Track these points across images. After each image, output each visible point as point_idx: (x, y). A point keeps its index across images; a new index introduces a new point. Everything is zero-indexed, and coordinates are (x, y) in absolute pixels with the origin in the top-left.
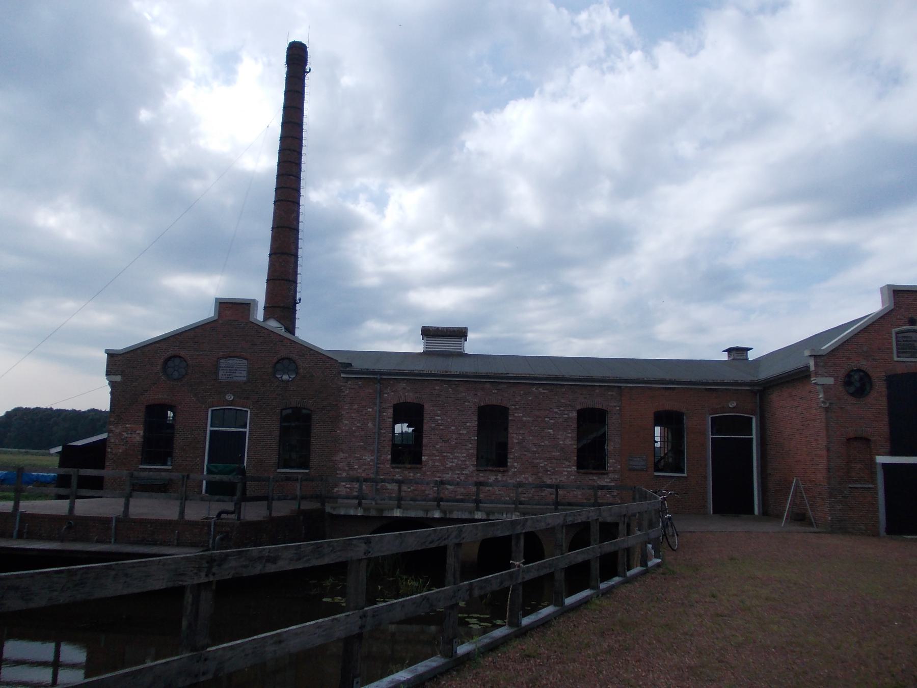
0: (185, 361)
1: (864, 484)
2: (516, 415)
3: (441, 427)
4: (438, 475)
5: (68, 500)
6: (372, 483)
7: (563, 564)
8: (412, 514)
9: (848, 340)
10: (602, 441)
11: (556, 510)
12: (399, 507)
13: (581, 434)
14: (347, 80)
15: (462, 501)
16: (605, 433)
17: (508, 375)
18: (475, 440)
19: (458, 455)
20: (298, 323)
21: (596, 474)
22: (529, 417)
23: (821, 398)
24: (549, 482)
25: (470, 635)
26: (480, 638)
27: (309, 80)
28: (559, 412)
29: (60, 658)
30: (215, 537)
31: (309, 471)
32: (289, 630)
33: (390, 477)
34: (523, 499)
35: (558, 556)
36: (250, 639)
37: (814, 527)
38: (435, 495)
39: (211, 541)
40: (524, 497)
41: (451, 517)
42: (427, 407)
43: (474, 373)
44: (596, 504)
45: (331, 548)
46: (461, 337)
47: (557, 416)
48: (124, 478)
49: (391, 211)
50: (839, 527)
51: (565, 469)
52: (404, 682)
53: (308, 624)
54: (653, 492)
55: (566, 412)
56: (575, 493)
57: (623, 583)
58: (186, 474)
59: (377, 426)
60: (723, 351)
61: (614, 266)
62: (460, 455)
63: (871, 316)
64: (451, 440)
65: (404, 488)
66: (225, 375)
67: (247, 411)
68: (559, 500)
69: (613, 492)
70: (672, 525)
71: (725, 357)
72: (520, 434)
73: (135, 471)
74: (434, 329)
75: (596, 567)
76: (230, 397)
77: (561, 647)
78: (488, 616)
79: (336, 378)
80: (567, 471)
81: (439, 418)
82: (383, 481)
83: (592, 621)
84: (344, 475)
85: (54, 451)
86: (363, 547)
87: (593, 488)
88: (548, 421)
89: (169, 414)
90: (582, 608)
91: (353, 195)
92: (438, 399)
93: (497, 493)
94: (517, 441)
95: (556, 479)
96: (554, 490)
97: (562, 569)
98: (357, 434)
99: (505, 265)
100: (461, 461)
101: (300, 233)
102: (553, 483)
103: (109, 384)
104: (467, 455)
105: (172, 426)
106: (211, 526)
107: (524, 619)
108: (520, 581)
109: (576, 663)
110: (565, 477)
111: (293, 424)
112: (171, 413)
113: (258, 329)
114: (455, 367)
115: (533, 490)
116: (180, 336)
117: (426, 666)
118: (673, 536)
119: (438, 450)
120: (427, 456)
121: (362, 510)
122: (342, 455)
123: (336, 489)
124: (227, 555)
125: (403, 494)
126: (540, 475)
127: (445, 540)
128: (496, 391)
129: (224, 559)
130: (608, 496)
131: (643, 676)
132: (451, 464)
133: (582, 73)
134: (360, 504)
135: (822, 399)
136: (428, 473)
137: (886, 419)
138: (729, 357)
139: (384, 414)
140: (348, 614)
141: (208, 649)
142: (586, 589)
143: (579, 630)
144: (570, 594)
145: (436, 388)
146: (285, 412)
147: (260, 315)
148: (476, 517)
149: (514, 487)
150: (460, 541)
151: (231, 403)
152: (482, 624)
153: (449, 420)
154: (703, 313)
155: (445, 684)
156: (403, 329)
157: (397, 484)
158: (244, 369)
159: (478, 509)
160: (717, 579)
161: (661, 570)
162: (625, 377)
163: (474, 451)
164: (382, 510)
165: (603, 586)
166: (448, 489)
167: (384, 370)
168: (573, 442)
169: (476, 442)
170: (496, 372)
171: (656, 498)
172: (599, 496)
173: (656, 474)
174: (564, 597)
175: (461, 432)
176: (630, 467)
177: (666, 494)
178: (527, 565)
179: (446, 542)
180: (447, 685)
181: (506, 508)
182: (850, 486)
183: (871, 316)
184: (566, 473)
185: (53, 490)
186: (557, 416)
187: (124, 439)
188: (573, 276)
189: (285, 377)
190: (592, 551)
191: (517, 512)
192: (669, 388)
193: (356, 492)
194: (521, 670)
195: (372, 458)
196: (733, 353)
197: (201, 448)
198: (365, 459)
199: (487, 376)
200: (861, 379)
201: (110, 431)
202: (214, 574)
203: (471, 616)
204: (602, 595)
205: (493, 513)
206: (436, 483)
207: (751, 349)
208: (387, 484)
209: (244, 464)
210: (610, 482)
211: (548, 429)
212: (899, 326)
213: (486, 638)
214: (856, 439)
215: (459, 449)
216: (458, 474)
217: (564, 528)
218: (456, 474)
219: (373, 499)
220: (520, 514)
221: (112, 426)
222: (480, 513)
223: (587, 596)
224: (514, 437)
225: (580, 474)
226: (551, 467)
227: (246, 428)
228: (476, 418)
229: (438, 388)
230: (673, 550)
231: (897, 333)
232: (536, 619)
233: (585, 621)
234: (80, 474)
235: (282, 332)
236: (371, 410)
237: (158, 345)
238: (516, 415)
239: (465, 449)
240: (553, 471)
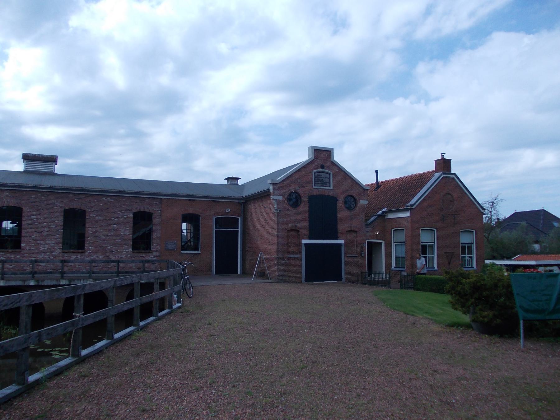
1: (295, 255)
2: (91, 215)
3: (36, 223)
4: (34, 256)
7: (114, 312)
8: (13, 284)
9: (290, 175)
11: (118, 276)
15: (51, 273)
16: (151, 228)
17: (85, 189)
18: (61, 232)
19: (48, 242)
21: (145, 253)
22: (101, 217)
23: (275, 207)
24: (113, 259)
28: (121, 214)
34: (96, 270)
37: (269, 279)
38: (31, 270)
40: (96, 269)
41: (43, 284)
43: (61, 186)
47: (120, 216)
50: (282, 279)
51: (125, 250)
54: (179, 263)
56: (131, 265)
57: (155, 321)
60: (225, 179)
61: (170, 120)
62: (50, 242)
63: (302, 163)
64: (44, 232)
65: (7, 265)
68: (119, 270)
69: (155, 264)
70: (189, 282)
71: (225, 182)
74: (32, 155)
75: (137, 312)
77: (108, 367)
78: (67, 349)
87: (142, 261)
88: (113, 219)
90: (126, 339)
92: (34, 204)
94: (91, 233)
95: (118, 257)
97: (113, 315)
100: (51, 246)
104: (56, 243)
108: (80, 326)
110: (125, 255)
114: (47, 182)
118: (190, 289)
127: (17, 303)
130: (152, 266)
131: (160, 380)
132: (43, 248)
135: (276, 208)
136: (25, 255)
137: (307, 219)
138: (228, 183)
142: (130, 327)
145: (32, 196)
148: (61, 283)
149: (89, 262)
150: (30, 303)
152: (61, 354)
153: (42, 218)
154: (222, 155)
159: (62, 278)
160: (213, 313)
161: (180, 310)
162: (165, 192)
163: (60, 240)
165: (142, 324)
168: (130, 233)
169: (62, 233)
170: (77, 187)
171: (180, 267)
173: (182, 252)
174: (113, 334)
176: (167, 248)
177: (186, 264)
179: (18, 305)
182: (288, 256)
183: (302, 163)
184: (125, 253)
186: (120, 216)
188: (144, 125)
190: (136, 302)
192: (191, 200)
196: (231, 180)
199: (71, 189)
200: (296, 197)
203: (54, 350)
204: (141, 330)
205: (74, 280)
206: (31, 262)
207: (241, 178)
210: (154, 258)
211: (114, 225)
212: (316, 169)
213: (53, 367)
214: (292, 230)
215: (50, 238)
217: (115, 289)
220: (93, 280)
223: (131, 331)
224: (90, 230)
225: (135, 253)
226: (115, 249)
228: (62, 217)
229: (34, 196)
230: (190, 297)
231: (315, 173)
232: (93, 350)
233: (127, 348)
238: (91, 215)
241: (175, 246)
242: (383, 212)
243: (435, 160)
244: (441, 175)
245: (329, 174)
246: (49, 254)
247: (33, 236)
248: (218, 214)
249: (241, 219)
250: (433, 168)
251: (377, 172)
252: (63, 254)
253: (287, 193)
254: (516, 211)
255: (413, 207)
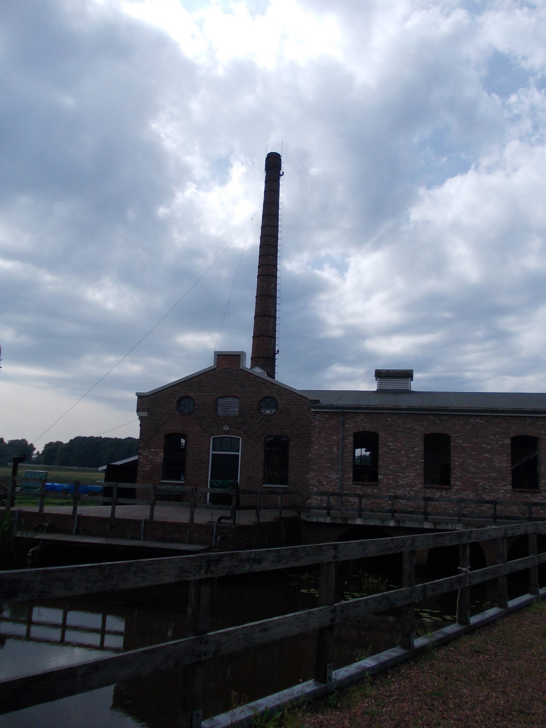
0: (193, 400)
5: (111, 506)
6: (338, 497)
8: (371, 523)
10: (534, 464)
12: (360, 516)
13: (514, 457)
14: (314, 171)
15: (412, 513)
18: (422, 462)
19: (407, 474)
20: (277, 369)
24: (487, 498)
25: (424, 629)
26: (434, 633)
27: (283, 181)
28: (495, 439)
29: (106, 627)
30: (216, 537)
31: (288, 487)
32: (272, 620)
33: (352, 492)
34: (465, 512)
35: (500, 565)
36: (241, 626)
39: (214, 540)
42: (381, 435)
44: (531, 519)
45: (305, 553)
46: (408, 377)
48: (150, 490)
49: (351, 277)
51: (502, 488)
52: (368, 669)
53: (288, 615)
55: (501, 439)
56: (511, 508)
58: (195, 487)
59: (341, 451)
62: (409, 474)
65: (364, 501)
66: (222, 411)
67: (240, 439)
72: (461, 457)
73: (158, 484)
76: (226, 428)
79: (307, 412)
80: (504, 490)
81: (392, 444)
82: (347, 495)
83: (533, 623)
84: (315, 490)
85: (101, 468)
86: (332, 552)
88: (485, 447)
89: (182, 441)
91: (319, 263)
92: (390, 428)
93: (443, 506)
95: (494, 496)
96: (492, 505)
98: (324, 457)
99: (447, 315)
100: (411, 479)
101: (278, 299)
102: (491, 499)
103: (139, 419)
105: (184, 450)
106: (213, 528)
107: (471, 618)
108: (467, 585)
109: (522, 661)
110: (502, 495)
111: (275, 449)
112: (184, 440)
113: (247, 374)
114: (404, 402)
115: (474, 504)
116: (189, 381)
117: (388, 656)
119: (391, 471)
120: (383, 475)
121: (330, 519)
122: (313, 474)
123: (309, 501)
124: (222, 556)
125: (363, 506)
126: (480, 492)
127: (400, 547)
128: (439, 422)
129: (219, 559)
133: (513, 145)
134: (328, 514)
136: (383, 489)
139: (346, 441)
140: (321, 608)
141: (209, 634)
143: (522, 630)
144: (511, 598)
146: (268, 440)
147: (248, 364)
151: (227, 432)
152: (433, 618)
153: (399, 446)
155: (404, 672)
156: (361, 371)
157: (358, 498)
158: (236, 406)
159: (426, 520)
163: (421, 472)
164: (346, 519)
166: (400, 503)
167: (345, 405)
172: (533, 512)
175: (410, 455)
178: (473, 572)
180: (406, 673)
181: (450, 519)
184: (503, 491)
185: (101, 498)
187: (150, 460)
189: (268, 412)
191: (460, 523)
193: (325, 504)
194: (472, 664)
195: (338, 476)
197: (205, 467)
198: (332, 477)
201: (139, 455)
202: (212, 572)
208: (350, 498)
209: (238, 480)
210: (543, 500)
216: (409, 490)
218: (406, 490)
219: (339, 510)
221: (141, 451)
222: (428, 523)
223: (528, 600)
224: (456, 460)
227: (239, 452)
228: (422, 444)
233: (527, 623)
234: (119, 487)
235: (265, 376)
236: (335, 437)
237: (173, 389)
238: (457, 441)
239: (414, 470)
240: (490, 489)
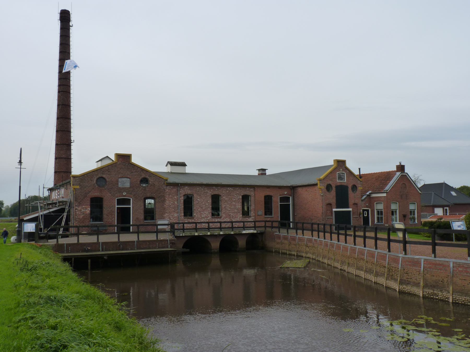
62: (206, 213)
95: (236, 219)
137: (335, 198)
228: (211, 199)
238: (223, 198)
241: (261, 213)
242: (370, 193)
243: (396, 166)
244: (400, 174)
245: (344, 174)
246: (206, 219)
247: (199, 210)
248: (280, 195)
249: (292, 198)
250: (395, 169)
251: (359, 169)
252: (212, 219)
253: (326, 185)
254: (71, 14)
255: (388, 191)
